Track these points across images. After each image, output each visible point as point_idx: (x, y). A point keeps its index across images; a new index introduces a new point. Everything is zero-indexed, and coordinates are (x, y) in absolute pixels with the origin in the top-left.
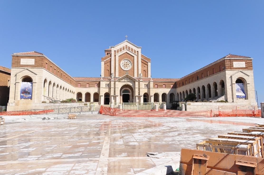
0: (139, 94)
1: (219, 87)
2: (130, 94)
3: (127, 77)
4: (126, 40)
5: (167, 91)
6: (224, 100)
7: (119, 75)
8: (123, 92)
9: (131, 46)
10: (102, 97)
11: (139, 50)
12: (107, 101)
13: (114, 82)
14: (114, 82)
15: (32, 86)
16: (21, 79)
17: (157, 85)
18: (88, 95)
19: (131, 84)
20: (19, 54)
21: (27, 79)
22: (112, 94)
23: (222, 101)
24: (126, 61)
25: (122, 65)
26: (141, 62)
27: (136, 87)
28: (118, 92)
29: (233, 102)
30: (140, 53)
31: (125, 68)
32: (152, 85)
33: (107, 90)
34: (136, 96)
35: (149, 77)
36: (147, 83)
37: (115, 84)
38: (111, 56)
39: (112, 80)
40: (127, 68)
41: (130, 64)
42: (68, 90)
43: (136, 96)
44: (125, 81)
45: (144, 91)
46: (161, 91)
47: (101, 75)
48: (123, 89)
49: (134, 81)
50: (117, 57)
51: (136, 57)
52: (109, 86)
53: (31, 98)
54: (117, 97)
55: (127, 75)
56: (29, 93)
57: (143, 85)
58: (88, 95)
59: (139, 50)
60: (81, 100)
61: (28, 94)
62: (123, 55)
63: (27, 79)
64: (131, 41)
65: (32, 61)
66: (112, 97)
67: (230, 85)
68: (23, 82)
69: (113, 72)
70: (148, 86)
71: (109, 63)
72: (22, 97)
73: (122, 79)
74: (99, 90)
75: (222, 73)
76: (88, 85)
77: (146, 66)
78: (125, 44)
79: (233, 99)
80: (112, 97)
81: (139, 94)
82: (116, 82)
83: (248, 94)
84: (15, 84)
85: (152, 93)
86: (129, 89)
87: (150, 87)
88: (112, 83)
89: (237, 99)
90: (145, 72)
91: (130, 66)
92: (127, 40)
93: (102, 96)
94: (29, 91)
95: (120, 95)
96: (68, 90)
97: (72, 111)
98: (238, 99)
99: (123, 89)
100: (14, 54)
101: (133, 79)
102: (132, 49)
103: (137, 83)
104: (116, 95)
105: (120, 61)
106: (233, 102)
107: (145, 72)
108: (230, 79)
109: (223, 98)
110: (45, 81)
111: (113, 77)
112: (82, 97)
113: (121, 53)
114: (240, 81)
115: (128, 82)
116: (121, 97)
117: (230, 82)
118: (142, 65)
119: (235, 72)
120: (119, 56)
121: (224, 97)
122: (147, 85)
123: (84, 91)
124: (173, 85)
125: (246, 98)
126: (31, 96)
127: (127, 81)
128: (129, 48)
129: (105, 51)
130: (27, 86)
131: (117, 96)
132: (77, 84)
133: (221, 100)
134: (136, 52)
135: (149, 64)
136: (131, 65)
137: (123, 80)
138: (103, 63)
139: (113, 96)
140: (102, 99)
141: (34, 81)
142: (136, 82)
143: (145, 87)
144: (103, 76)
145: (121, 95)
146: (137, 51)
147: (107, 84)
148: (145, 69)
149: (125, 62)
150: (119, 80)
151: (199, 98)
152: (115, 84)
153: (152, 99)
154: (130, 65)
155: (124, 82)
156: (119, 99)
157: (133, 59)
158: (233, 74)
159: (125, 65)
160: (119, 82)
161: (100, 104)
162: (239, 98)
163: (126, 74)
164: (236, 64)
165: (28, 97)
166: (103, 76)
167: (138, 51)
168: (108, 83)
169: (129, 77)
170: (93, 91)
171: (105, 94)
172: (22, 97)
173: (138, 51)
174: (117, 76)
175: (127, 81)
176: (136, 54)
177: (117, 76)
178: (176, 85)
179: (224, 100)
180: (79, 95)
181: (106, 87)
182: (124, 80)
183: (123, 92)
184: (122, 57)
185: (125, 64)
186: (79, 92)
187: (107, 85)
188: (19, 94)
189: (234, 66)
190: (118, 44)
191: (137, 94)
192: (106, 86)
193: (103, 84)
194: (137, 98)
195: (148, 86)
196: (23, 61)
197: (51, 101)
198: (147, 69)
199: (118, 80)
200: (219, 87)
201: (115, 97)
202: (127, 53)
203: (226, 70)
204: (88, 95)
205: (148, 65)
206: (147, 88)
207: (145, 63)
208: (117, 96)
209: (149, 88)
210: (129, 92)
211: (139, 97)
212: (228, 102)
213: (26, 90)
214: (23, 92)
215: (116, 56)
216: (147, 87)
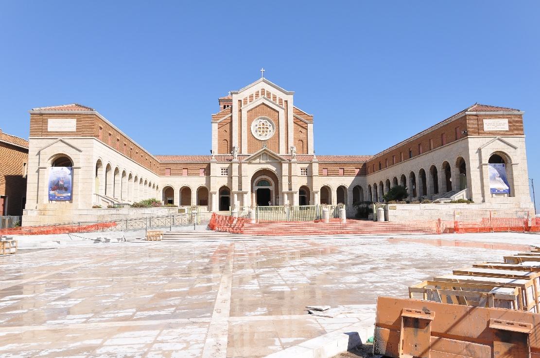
0: (290, 189)
1: (454, 171)
2: (272, 188)
3: (266, 154)
4: (261, 79)
5: (348, 182)
6: (466, 199)
7: (249, 151)
8: (258, 185)
9: (268, 88)
10: (214, 196)
11: (290, 98)
12: (225, 204)
13: (238, 165)
14: (238, 165)
15: (72, 174)
16: (50, 161)
17: (331, 167)
18: (186, 191)
19: (273, 168)
20: (44, 109)
21: (62, 161)
22: (235, 188)
23: (460, 201)
24: (263, 121)
25: (254, 128)
28: (247, 186)
30: (291, 105)
32: (316, 168)
33: (224, 182)
34: (283, 194)
35: (311, 152)
36: (306, 166)
37: (240, 168)
38: (231, 112)
39: (234, 160)
40: (264, 134)
41: (271, 126)
42: (136, 177)
44: (262, 161)
45: (299, 181)
46: (334, 183)
47: (211, 151)
48: (258, 179)
49: (279, 162)
51: (282, 113)
52: (228, 172)
53: (70, 199)
54: (245, 196)
55: (265, 150)
56: (66, 189)
57: (297, 169)
58: (186, 192)
59: (290, 98)
60: (171, 202)
61: (64, 191)
63: (62, 161)
65: (70, 125)
66: (236, 196)
68: (53, 166)
69: (235, 143)
70: (308, 172)
72: (52, 198)
73: (255, 159)
74: (208, 181)
75: (460, 144)
77: (304, 131)
78: (260, 85)
79: (483, 196)
80: (236, 196)
81: (290, 189)
84: (38, 171)
85: (317, 185)
86: (270, 179)
88: (235, 167)
90: (303, 143)
94: (65, 186)
95: (252, 191)
96: (136, 177)
97: (153, 223)
98: (494, 195)
99: (258, 179)
100: (34, 109)
103: (285, 166)
104: (243, 190)
106: (484, 201)
107: (303, 143)
109: (462, 195)
110: (99, 164)
111: (236, 154)
113: (251, 106)
114: (497, 159)
115: (267, 163)
116: (254, 195)
119: (488, 140)
122: (227, 170)
123: (177, 183)
124: (359, 170)
125: (510, 193)
126: (69, 194)
127: (264, 162)
128: (269, 94)
129: (220, 101)
130: (61, 175)
131: (246, 193)
132: (167, 168)
133: (459, 198)
134: (284, 101)
135: (310, 127)
136: (273, 129)
137: (258, 161)
138: (215, 126)
139: (238, 194)
140: (215, 200)
141: (75, 165)
143: (303, 173)
144: (216, 152)
145: (254, 191)
147: (304, 169)
148: (302, 136)
149: (261, 123)
152: (240, 168)
153: (318, 198)
154: (271, 128)
155: (260, 163)
156: (250, 199)
157: (276, 117)
158: (484, 146)
159: (263, 129)
160: (250, 163)
161: (210, 209)
162: (496, 194)
164: (489, 125)
165: (65, 197)
166: (216, 152)
167: (286, 101)
168: (227, 166)
169: (268, 153)
170: (195, 183)
171: (220, 189)
172: (52, 198)
173: (286, 101)
174: (245, 151)
175: (264, 162)
176: (284, 107)
177: (245, 151)
178: (365, 170)
179: (466, 199)
180: (168, 192)
184: (253, 113)
187: (303, 171)
188: (45, 191)
189: (487, 128)
190: (246, 87)
191: (285, 188)
193: (216, 169)
195: (308, 172)
196: (53, 125)
197: (111, 204)
198: (305, 136)
200: (454, 171)
201: (241, 195)
202: (263, 104)
203: (468, 136)
204: (186, 191)
205: (307, 129)
208: (246, 193)
209: (310, 177)
210: (269, 184)
211: (291, 195)
212: (473, 202)
213: (61, 183)
214: (53, 186)
216: (305, 173)
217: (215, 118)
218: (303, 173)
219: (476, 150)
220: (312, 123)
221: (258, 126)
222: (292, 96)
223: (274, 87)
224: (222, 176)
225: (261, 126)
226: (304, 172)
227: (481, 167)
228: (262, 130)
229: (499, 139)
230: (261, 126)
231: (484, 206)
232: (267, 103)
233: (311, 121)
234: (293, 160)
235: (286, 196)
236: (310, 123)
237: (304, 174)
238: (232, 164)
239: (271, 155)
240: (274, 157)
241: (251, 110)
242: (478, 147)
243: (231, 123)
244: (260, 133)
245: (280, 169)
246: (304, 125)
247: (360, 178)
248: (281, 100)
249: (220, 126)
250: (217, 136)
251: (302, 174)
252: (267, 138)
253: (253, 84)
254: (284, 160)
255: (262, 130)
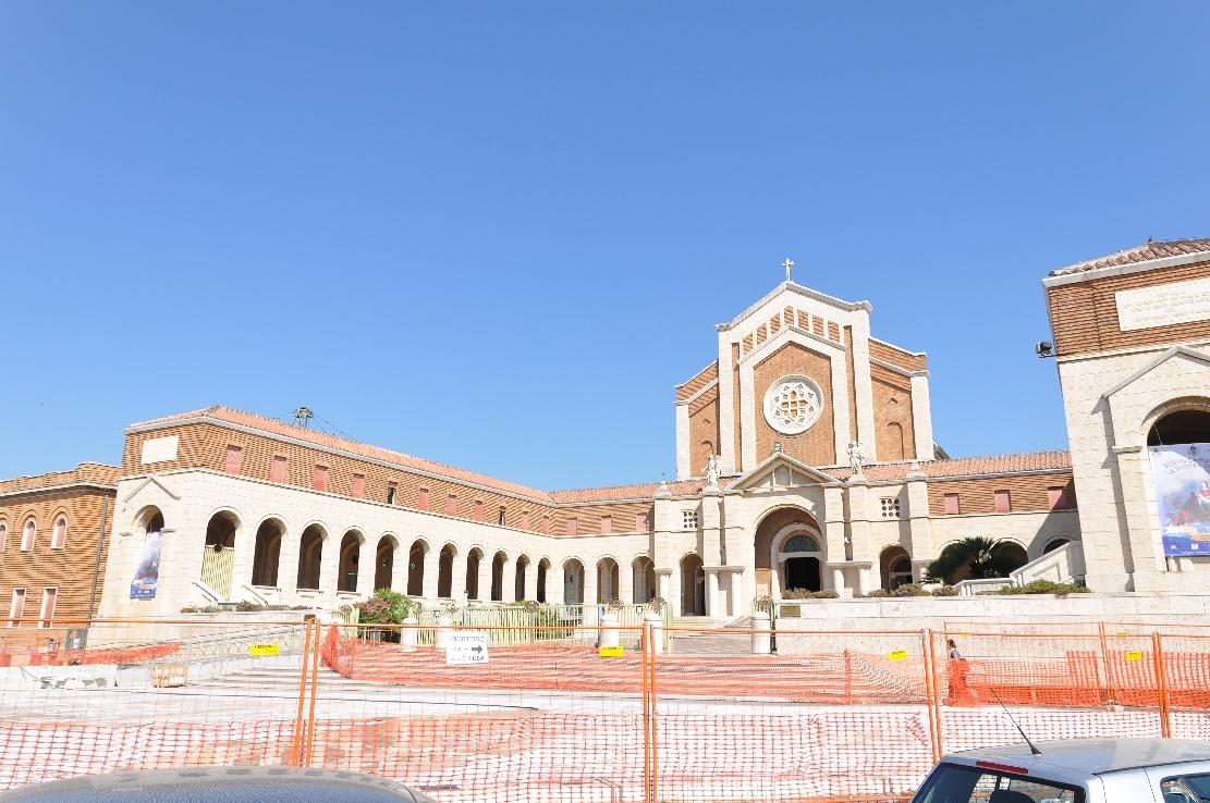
3: (782, 469)
4: (783, 285)
6: (1068, 580)
8: (786, 548)
9: (813, 308)
12: (695, 602)
14: (841, 491)
18: (609, 568)
19: (806, 504)
22: (711, 560)
23: (1041, 588)
24: (793, 386)
26: (873, 378)
27: (912, 515)
28: (743, 550)
29: (1130, 587)
31: (787, 422)
32: (919, 498)
33: (688, 545)
36: (893, 492)
40: (797, 418)
41: (815, 396)
43: (833, 568)
45: (873, 540)
49: (814, 484)
50: (747, 374)
51: (839, 360)
55: (779, 458)
57: (868, 503)
59: (860, 321)
62: (778, 358)
64: (813, 280)
67: (1105, 466)
70: (899, 506)
71: (714, 404)
73: (758, 484)
74: (906, 533)
76: (609, 520)
77: (900, 396)
81: (849, 558)
82: (909, 484)
83: (1082, 530)
86: (800, 527)
87: (908, 511)
89: (1179, 570)
90: (899, 430)
91: (811, 409)
92: (792, 283)
93: (868, 567)
101: (815, 478)
102: (818, 322)
103: (832, 497)
105: (760, 391)
107: (899, 430)
108: (1099, 417)
112: (910, 570)
117: (1103, 443)
118: (877, 397)
119: (1140, 362)
120: (755, 368)
121: (1064, 553)
122: (897, 501)
124: (1060, 492)
127: (783, 489)
128: (803, 317)
135: (920, 385)
137: (766, 487)
138: (682, 413)
139: (844, 570)
140: (671, 588)
142: (826, 490)
143: (887, 512)
146: (846, 328)
147: (890, 501)
148: (899, 412)
149: (790, 391)
150: (746, 488)
151: (642, 593)
154: (813, 401)
159: (792, 406)
160: (747, 494)
163: (775, 456)
167: (848, 328)
170: (626, 549)
173: (848, 328)
175: (783, 489)
176: (842, 343)
179: (1068, 580)
181: (884, 515)
182: (768, 484)
183: (786, 548)
185: (789, 400)
186: (950, 546)
187: (887, 505)
189: (1127, 322)
190: (748, 312)
192: (884, 508)
193: (670, 515)
194: (839, 577)
195: (899, 506)
199: (737, 487)
202: (791, 343)
204: (609, 568)
206: (895, 517)
207: (892, 381)
209: (905, 521)
212: (1087, 591)
215: (742, 370)
216: (894, 511)
217: (682, 392)
218: (887, 512)
219: (1095, 403)
220: (924, 374)
221: (782, 400)
222: (863, 314)
223: (806, 295)
224: (686, 529)
225: (789, 400)
226: (691, 520)
227: (1112, 462)
228: (790, 408)
229: (1181, 354)
230: (799, 398)
231: (1129, 607)
232: (799, 339)
233: (920, 366)
234: (853, 479)
235: (839, 577)
236: (919, 375)
237: (891, 514)
238: (846, 489)
239: (797, 469)
240: (806, 474)
241: (763, 362)
242: (1104, 391)
243: (717, 400)
244: (807, 410)
245: (820, 505)
246: (901, 383)
247: (1062, 515)
248: (834, 328)
249: (693, 412)
250: (679, 440)
251: (686, 526)
252: (806, 426)
253: (764, 300)
254: (826, 480)
255: (790, 408)
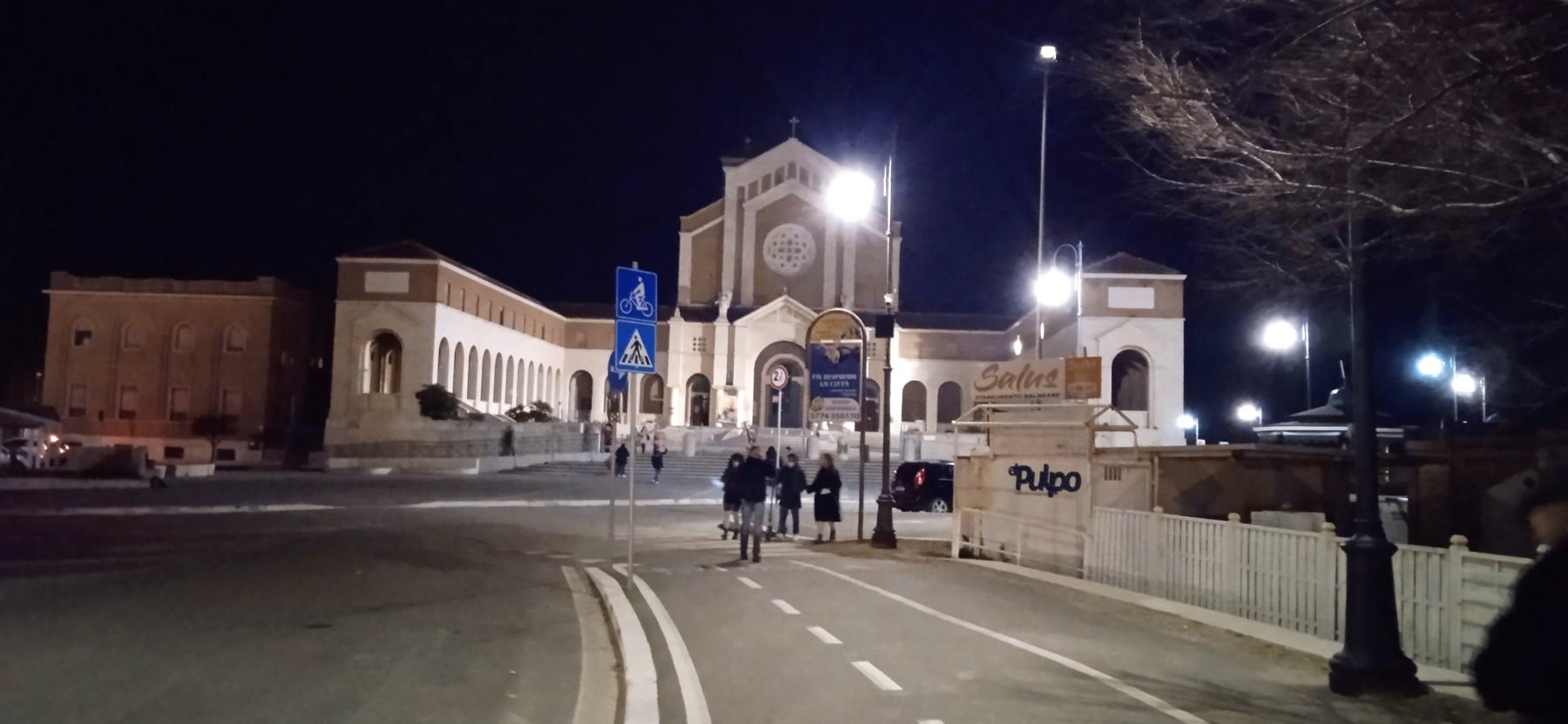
25: (769, 252)
105: (762, 231)
